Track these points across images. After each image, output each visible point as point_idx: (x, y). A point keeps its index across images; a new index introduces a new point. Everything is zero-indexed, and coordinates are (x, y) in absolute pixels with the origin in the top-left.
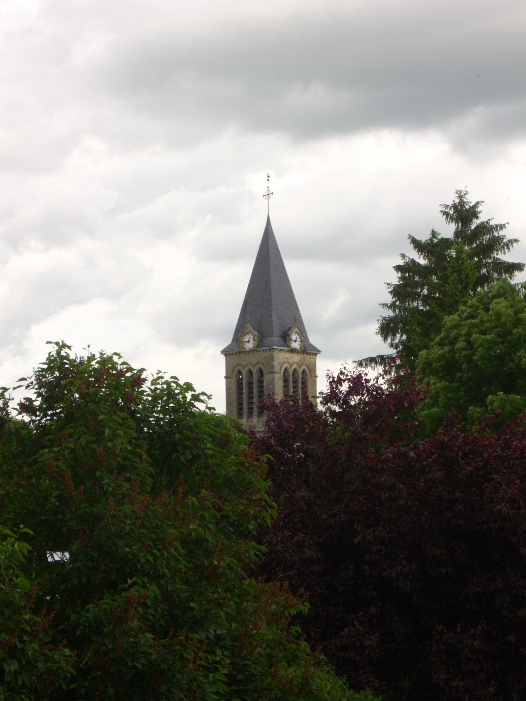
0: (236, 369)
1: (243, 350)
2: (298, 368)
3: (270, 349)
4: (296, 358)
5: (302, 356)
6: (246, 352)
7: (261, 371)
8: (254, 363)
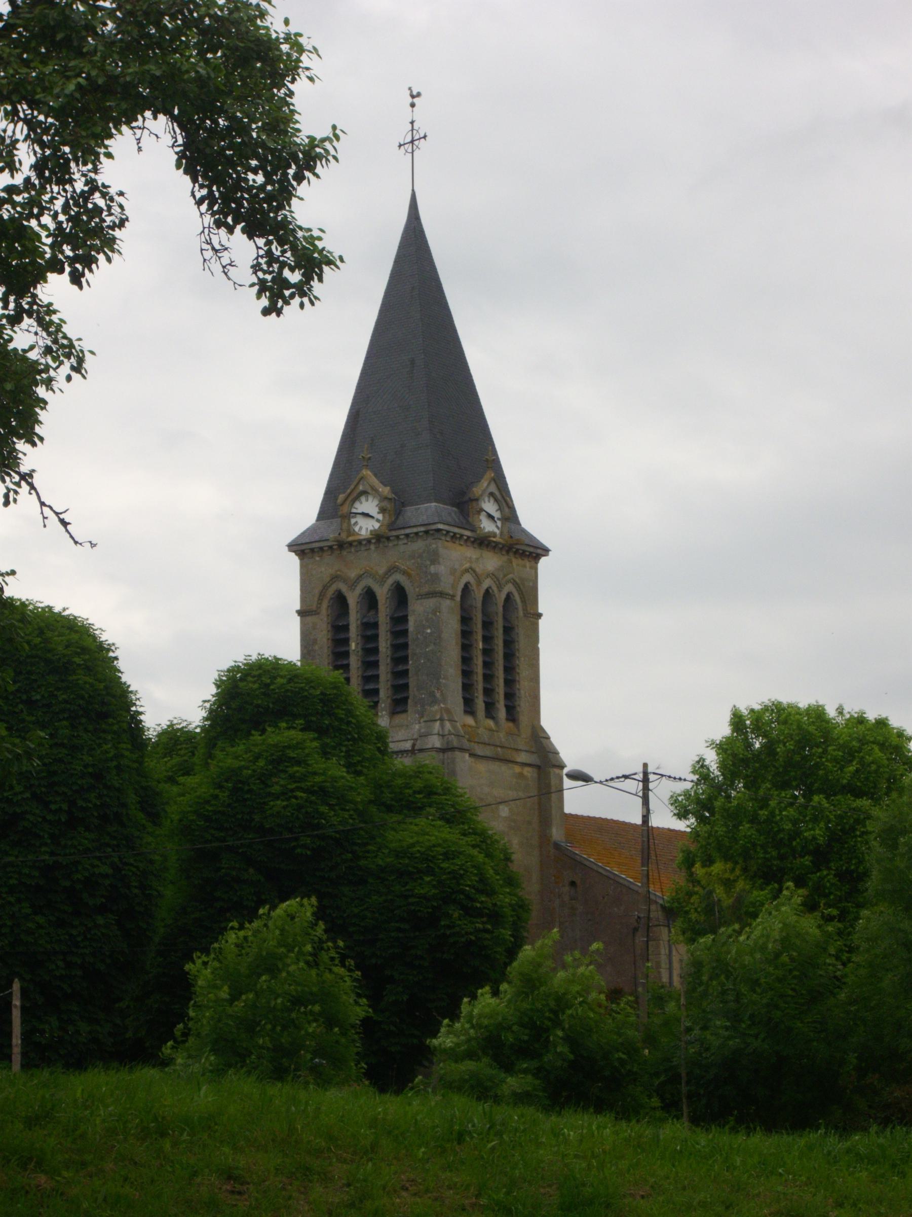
0: (334, 587)
1: (351, 539)
2: (495, 588)
3: (427, 532)
4: (491, 562)
5: (505, 558)
6: (360, 542)
7: (400, 595)
8: (381, 571)
